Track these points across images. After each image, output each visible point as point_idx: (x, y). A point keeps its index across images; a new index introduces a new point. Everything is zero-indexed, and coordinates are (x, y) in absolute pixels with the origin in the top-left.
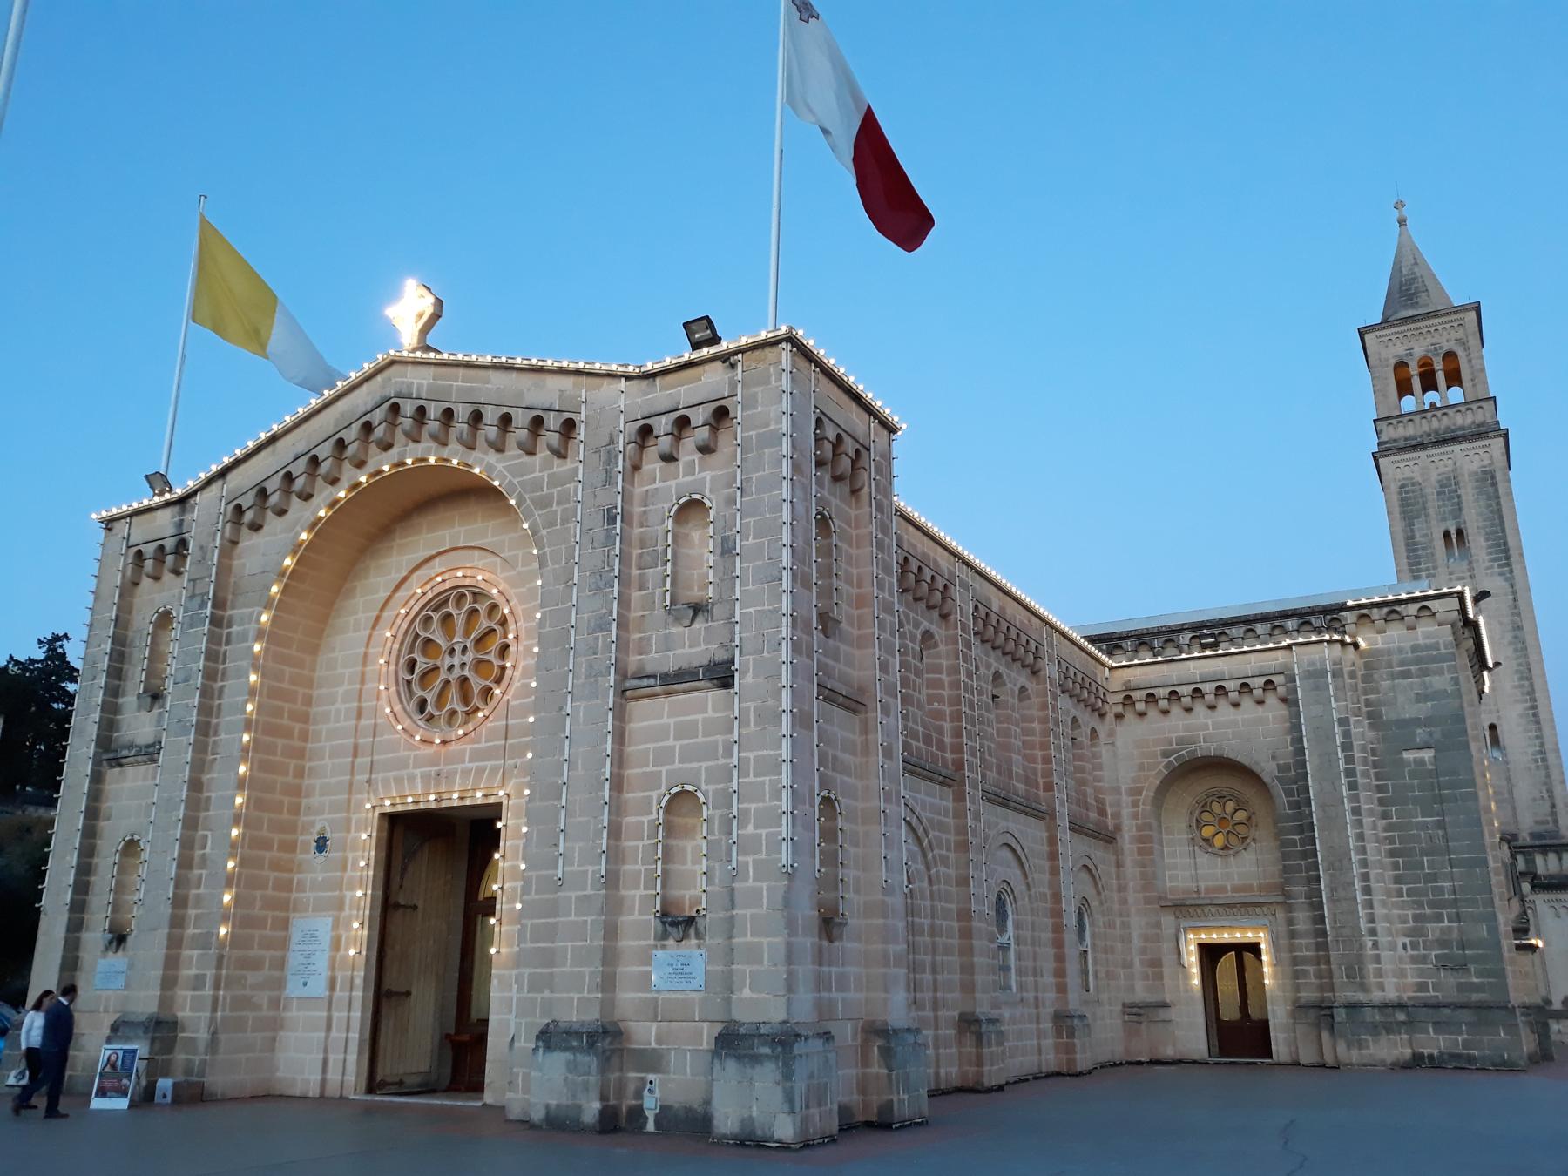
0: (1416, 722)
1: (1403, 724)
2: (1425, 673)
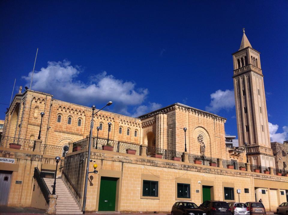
0: (171, 124)
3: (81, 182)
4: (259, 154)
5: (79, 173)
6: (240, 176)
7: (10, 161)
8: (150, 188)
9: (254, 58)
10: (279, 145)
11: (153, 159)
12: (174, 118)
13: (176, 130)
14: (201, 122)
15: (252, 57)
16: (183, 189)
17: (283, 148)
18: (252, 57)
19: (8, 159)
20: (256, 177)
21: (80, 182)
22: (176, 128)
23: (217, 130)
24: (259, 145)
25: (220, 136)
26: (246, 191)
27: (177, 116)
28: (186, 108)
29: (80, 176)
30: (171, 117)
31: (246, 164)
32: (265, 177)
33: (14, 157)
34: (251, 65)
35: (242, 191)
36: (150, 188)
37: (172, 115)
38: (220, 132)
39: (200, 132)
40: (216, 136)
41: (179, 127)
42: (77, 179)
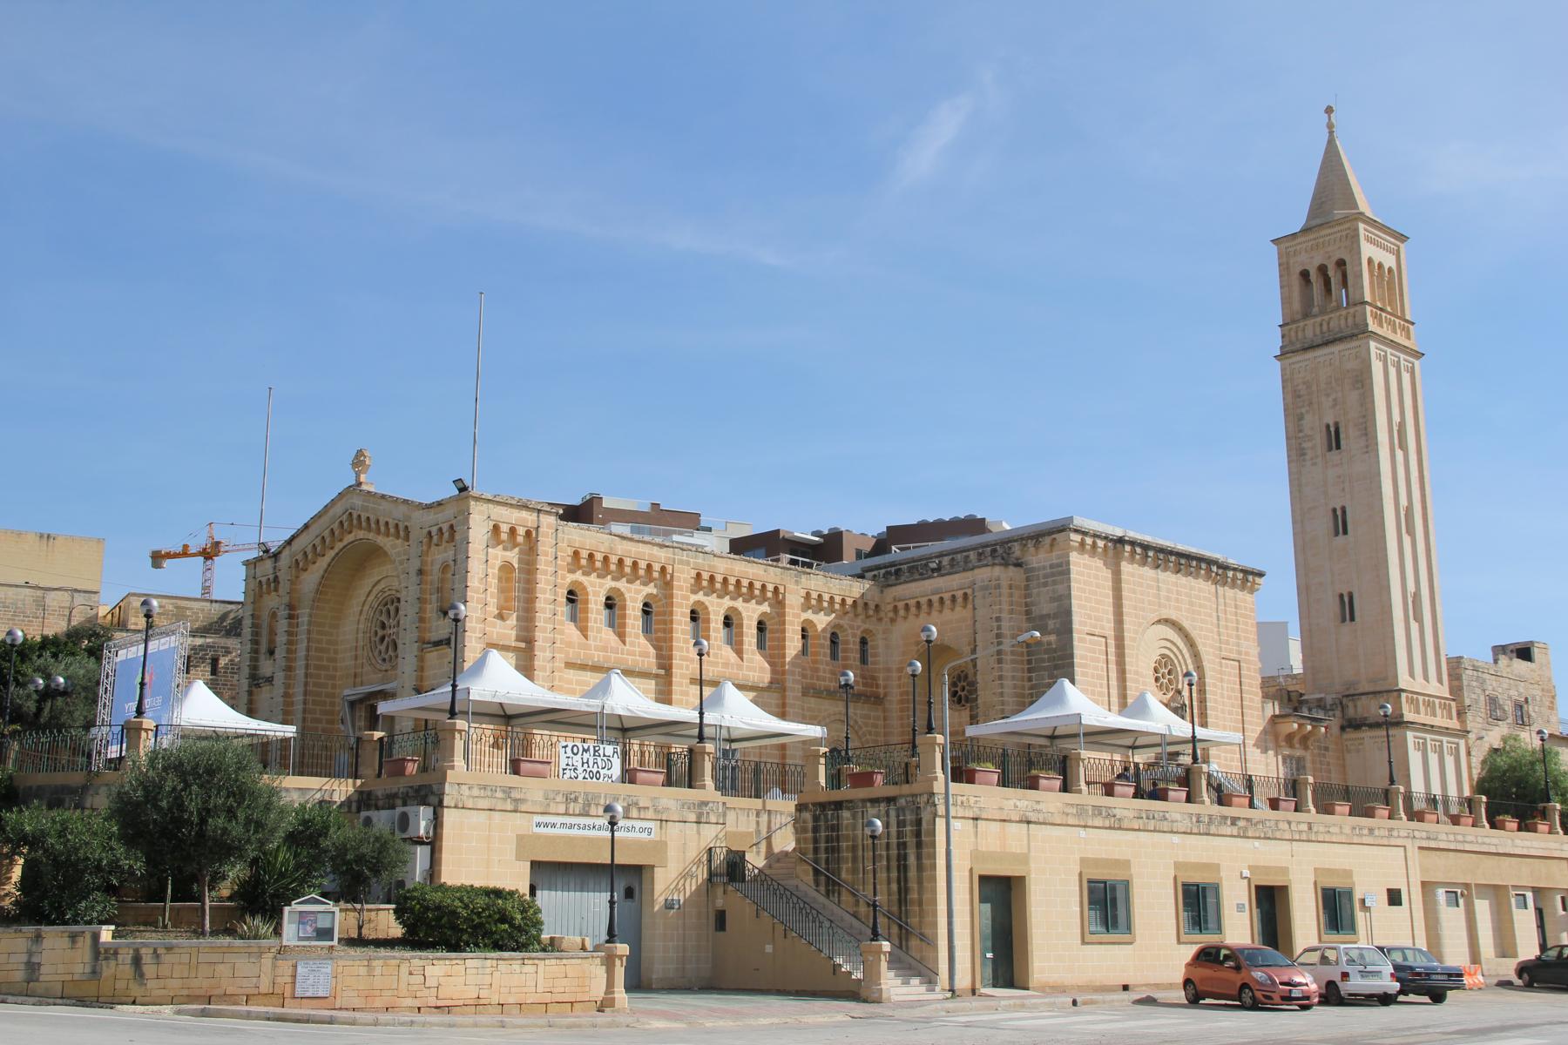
0: (1048, 616)
1: (1042, 617)
2: (1055, 583)
3: (920, 892)
4: (1397, 722)
5: (905, 867)
6: (1370, 840)
7: (642, 830)
8: (1107, 904)
9: (1380, 265)
10: (1475, 669)
11: (1109, 801)
12: (1060, 588)
13: (1075, 643)
14: (1168, 599)
15: (1370, 261)
16: (1197, 902)
17: (1492, 685)
18: (1370, 261)
19: (638, 824)
20: (1425, 844)
21: (914, 895)
22: (1075, 635)
23: (1227, 627)
24: (1401, 686)
25: (1239, 653)
26: (1394, 898)
27: (1079, 582)
28: (1099, 537)
29: (912, 873)
30: (1045, 584)
31: (1387, 792)
32: (1456, 841)
33: (650, 814)
34: (1368, 308)
35: (1378, 901)
36: (1107, 904)
37: (1053, 575)
38: (1238, 637)
39: (1169, 645)
40: (1224, 654)
41: (1087, 629)
42: (894, 887)
